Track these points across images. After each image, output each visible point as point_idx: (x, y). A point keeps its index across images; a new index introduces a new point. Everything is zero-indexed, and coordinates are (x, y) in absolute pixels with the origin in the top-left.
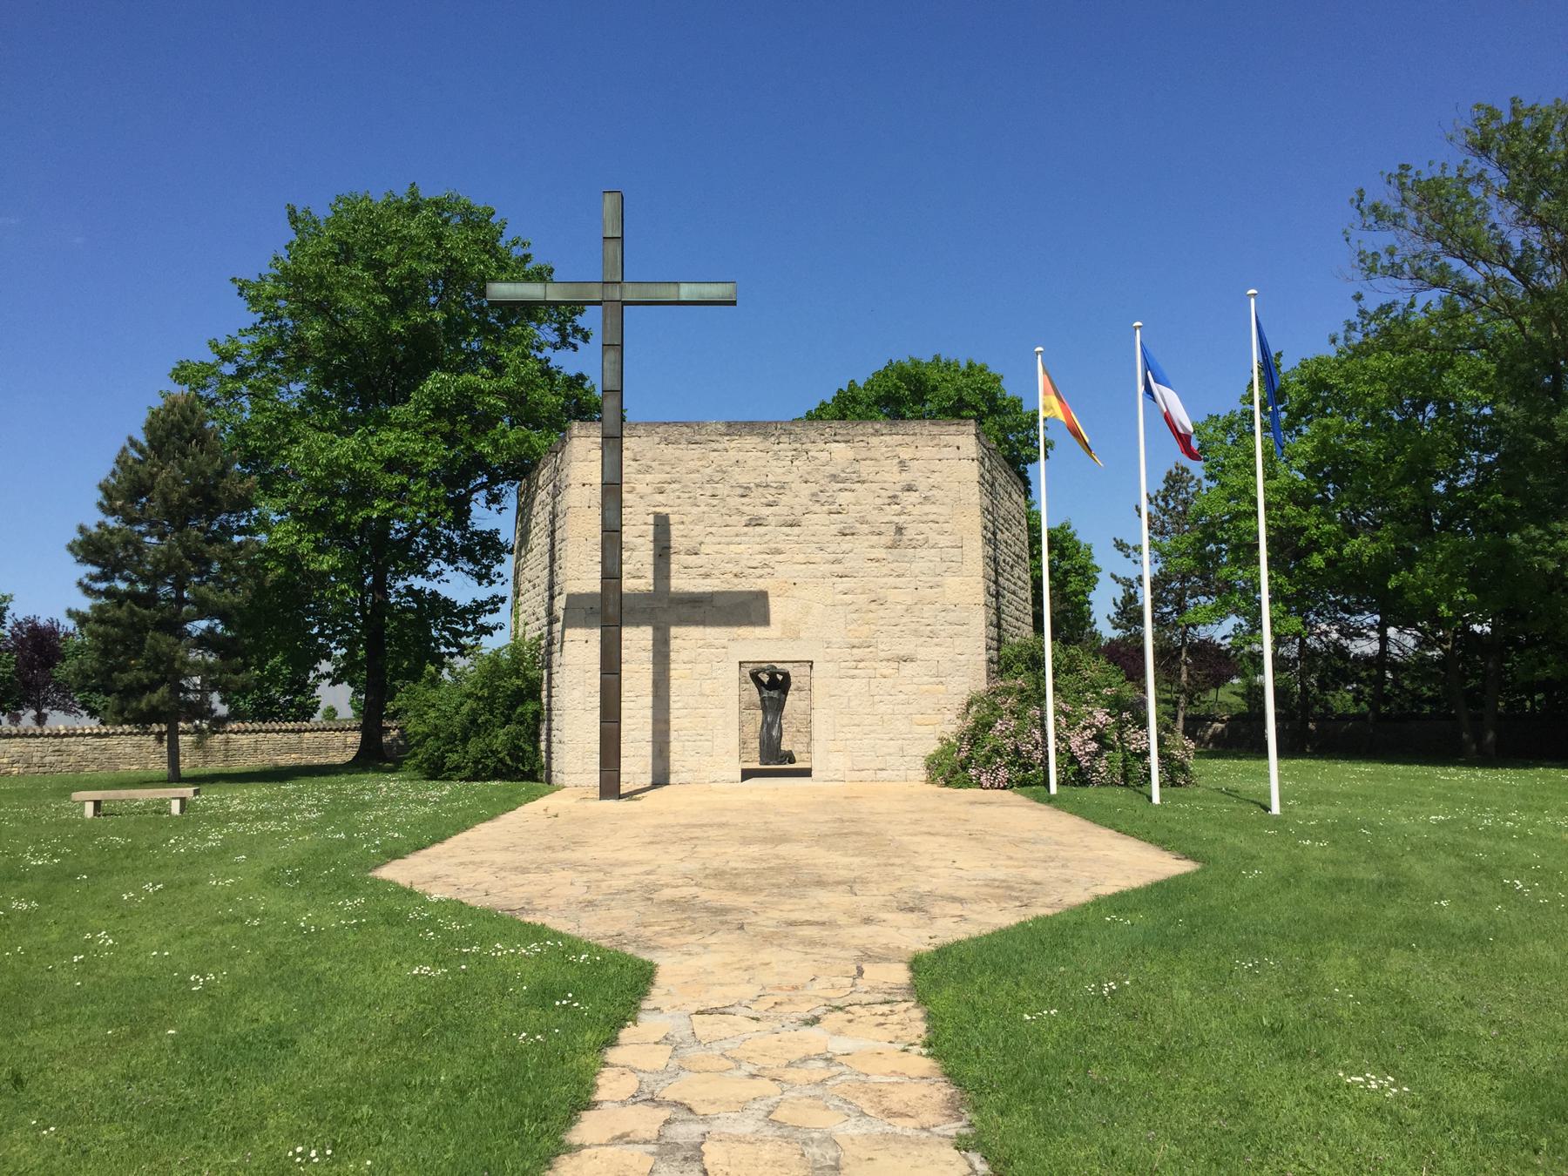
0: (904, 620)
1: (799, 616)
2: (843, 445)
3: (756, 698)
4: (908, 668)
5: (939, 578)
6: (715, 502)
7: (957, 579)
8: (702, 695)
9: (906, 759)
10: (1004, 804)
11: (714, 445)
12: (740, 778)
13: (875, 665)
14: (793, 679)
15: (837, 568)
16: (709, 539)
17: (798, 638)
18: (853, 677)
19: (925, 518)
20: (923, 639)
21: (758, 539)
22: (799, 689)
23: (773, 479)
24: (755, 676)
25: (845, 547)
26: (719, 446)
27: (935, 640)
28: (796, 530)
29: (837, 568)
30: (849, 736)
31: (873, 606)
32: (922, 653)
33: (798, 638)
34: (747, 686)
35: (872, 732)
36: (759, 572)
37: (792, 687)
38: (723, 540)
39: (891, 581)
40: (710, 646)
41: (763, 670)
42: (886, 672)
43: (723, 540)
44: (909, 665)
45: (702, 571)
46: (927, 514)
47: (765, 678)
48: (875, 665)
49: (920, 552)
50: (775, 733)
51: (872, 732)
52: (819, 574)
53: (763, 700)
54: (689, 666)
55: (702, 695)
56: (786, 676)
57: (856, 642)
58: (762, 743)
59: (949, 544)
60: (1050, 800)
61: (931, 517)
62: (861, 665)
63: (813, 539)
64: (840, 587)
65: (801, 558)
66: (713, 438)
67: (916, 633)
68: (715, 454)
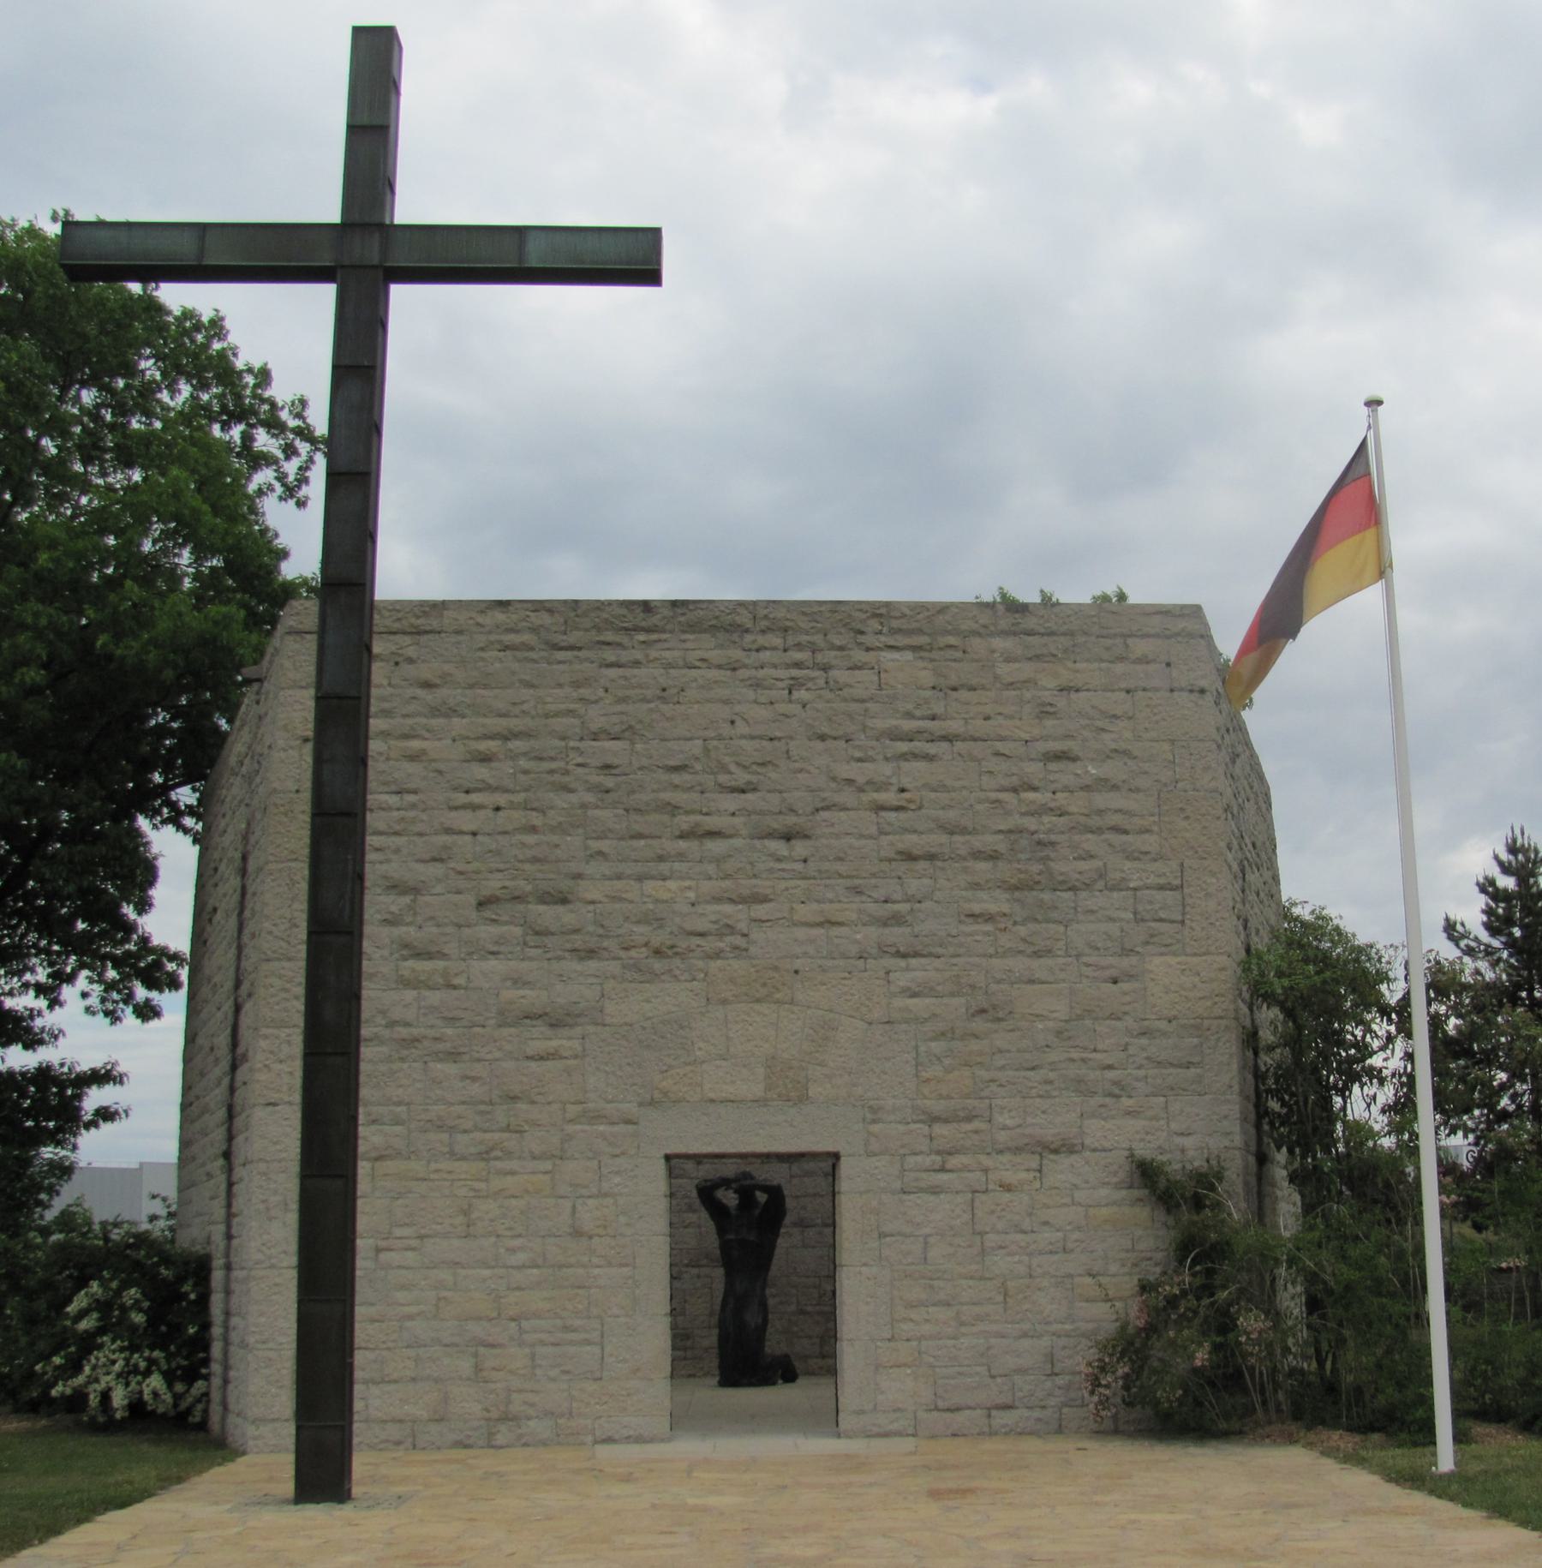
0: (1053, 1056)
1: (819, 1221)
2: (909, 655)
3: (712, 1241)
4: (1061, 1170)
5: (1134, 960)
6: (610, 782)
7: (1172, 960)
8: (577, 1233)
9: (1060, 1381)
10: (1398, 1512)
11: (610, 655)
12: (289, 1488)
13: (986, 1161)
14: (790, 1203)
15: (897, 936)
16: (592, 869)
17: (803, 1098)
18: (935, 1190)
19: (1095, 821)
20: (1099, 1100)
21: (711, 869)
22: (802, 1224)
23: (746, 730)
24: (707, 1193)
25: (914, 886)
26: (625, 656)
27: (1126, 1102)
28: (800, 848)
29: (897, 936)
30: (926, 1329)
31: (979, 1025)
32: (1097, 1131)
33: (803, 1098)
34: (692, 1217)
35: (979, 1318)
36: (710, 944)
37: (788, 1220)
38: (630, 868)
39: (1019, 964)
40: (597, 1117)
41: (725, 1182)
42: (1010, 1177)
43: (630, 868)
44: (1065, 1161)
45: (578, 941)
46: (1100, 812)
47: (730, 1198)
48: (986, 1161)
49: (1087, 900)
50: (752, 1318)
51: (979, 1318)
52: (854, 950)
53: (725, 1247)
54: (548, 1165)
55: (577, 1233)
56: (776, 1194)
57: (938, 1107)
58: (723, 1339)
59: (1152, 880)
60: (1439, 1487)
61: (1116, 819)
62: (953, 1162)
63: (841, 868)
64: (901, 980)
65: (804, 912)
66: (609, 636)
67: (1081, 1087)
68: (613, 673)
